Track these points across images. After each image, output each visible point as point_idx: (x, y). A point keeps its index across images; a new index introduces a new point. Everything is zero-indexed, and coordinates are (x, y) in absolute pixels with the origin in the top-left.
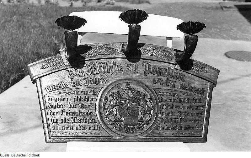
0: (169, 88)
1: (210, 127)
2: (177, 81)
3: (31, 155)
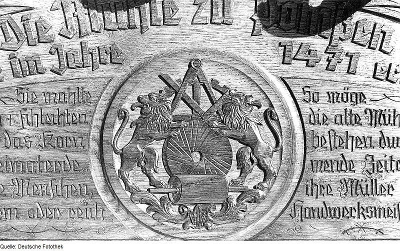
0: (335, 77)
1: (205, 241)
2: (365, 50)
3: (49, 247)
